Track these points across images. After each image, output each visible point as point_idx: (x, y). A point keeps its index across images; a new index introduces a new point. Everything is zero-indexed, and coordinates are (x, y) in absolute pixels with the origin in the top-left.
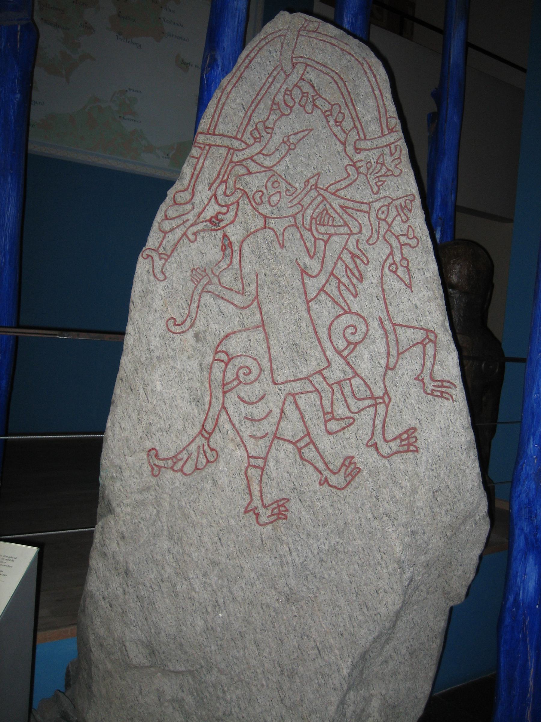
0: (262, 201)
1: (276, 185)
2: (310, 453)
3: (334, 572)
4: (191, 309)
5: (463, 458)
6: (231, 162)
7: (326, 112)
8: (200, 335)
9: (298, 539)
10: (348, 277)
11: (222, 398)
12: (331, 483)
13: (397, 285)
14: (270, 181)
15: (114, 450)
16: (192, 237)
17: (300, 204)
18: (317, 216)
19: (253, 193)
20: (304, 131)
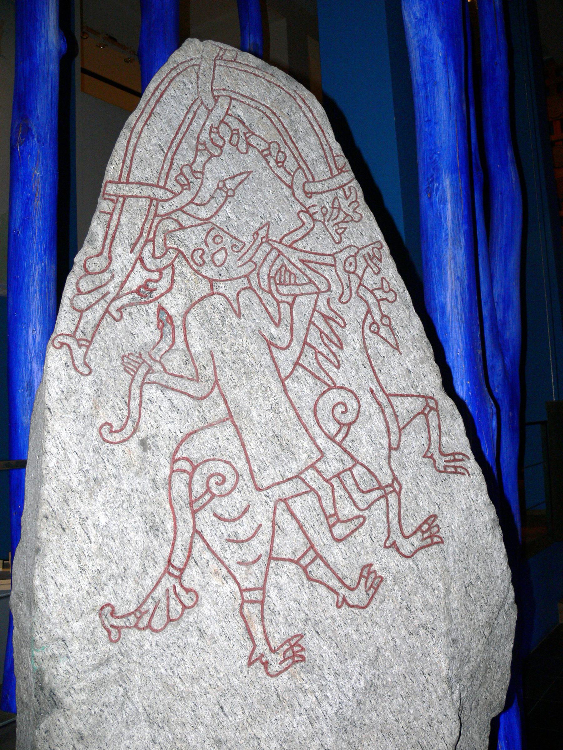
0: (204, 261)
1: (218, 240)
2: (319, 571)
3: (375, 714)
4: (131, 409)
5: (489, 540)
6: (156, 215)
7: (263, 151)
8: (148, 441)
9: (324, 683)
10: (325, 344)
11: (191, 520)
12: (351, 603)
13: (382, 347)
14: (210, 235)
15: (51, 617)
16: (116, 315)
17: (252, 262)
18: (276, 274)
19: (191, 251)
20: (240, 174)
